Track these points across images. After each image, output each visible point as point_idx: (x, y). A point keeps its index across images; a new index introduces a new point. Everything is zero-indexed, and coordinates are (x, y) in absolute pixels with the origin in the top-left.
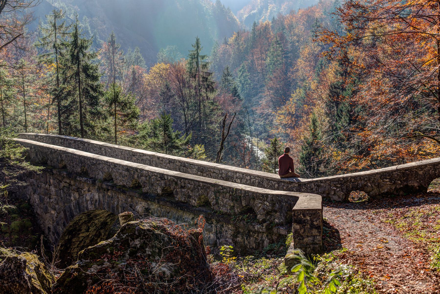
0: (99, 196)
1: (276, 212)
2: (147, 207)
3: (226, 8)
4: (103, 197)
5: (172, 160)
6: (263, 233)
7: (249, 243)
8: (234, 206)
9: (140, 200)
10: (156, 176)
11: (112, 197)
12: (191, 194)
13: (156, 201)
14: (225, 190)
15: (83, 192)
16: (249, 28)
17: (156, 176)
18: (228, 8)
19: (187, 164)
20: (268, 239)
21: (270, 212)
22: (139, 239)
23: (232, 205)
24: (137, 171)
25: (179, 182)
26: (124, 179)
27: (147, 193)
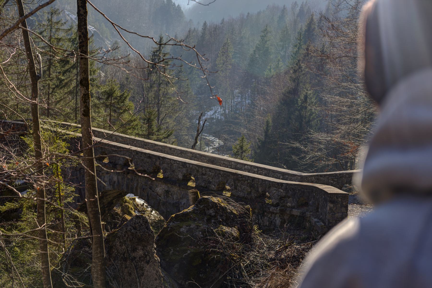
0: (118, 178)
1: (289, 197)
2: (166, 189)
3: (177, 5)
4: (122, 179)
5: (184, 151)
6: (276, 213)
7: (263, 221)
8: (251, 192)
9: (160, 183)
10: (178, 164)
11: (132, 180)
12: (211, 181)
13: (178, 185)
14: (244, 179)
15: (101, 174)
16: (200, 29)
17: (178, 164)
18: (178, 6)
19: (198, 156)
20: (280, 219)
21: (283, 197)
22: (213, 209)
23: (249, 190)
24: (159, 159)
25: (200, 170)
26: (145, 165)
27: (168, 177)
